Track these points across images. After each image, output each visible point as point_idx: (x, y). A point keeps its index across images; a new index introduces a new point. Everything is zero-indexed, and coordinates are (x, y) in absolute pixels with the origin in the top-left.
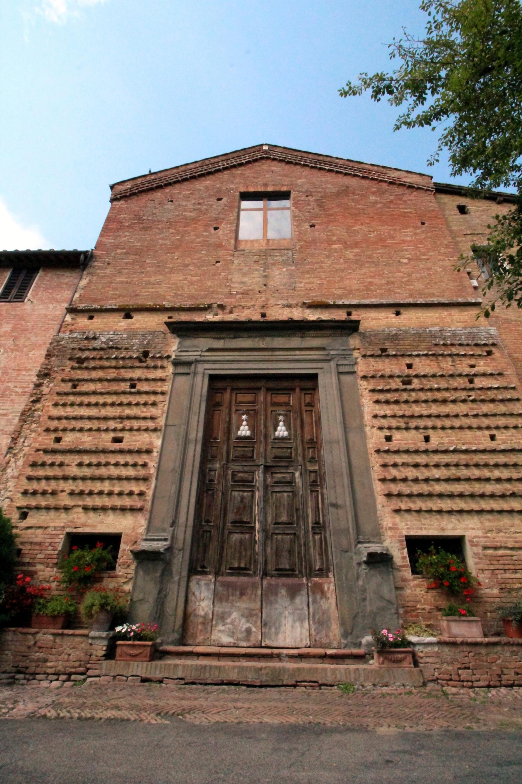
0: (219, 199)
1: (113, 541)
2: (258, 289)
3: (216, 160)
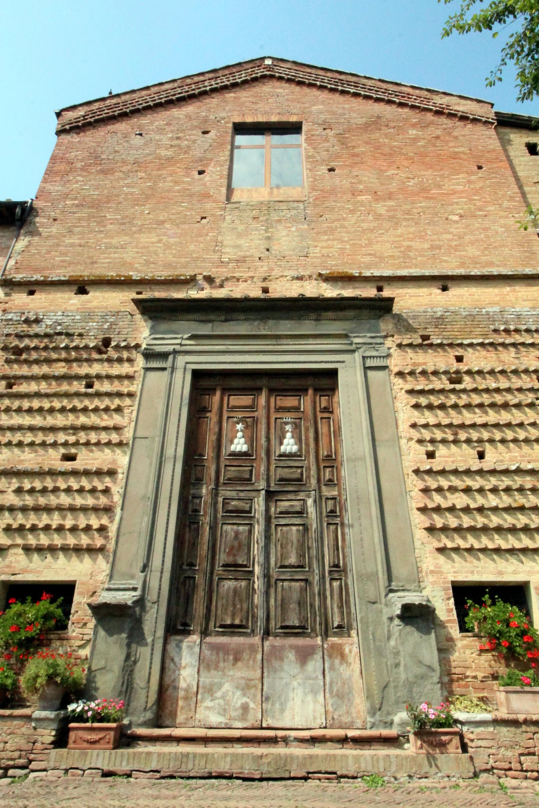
0: (205, 133)
3: (201, 78)
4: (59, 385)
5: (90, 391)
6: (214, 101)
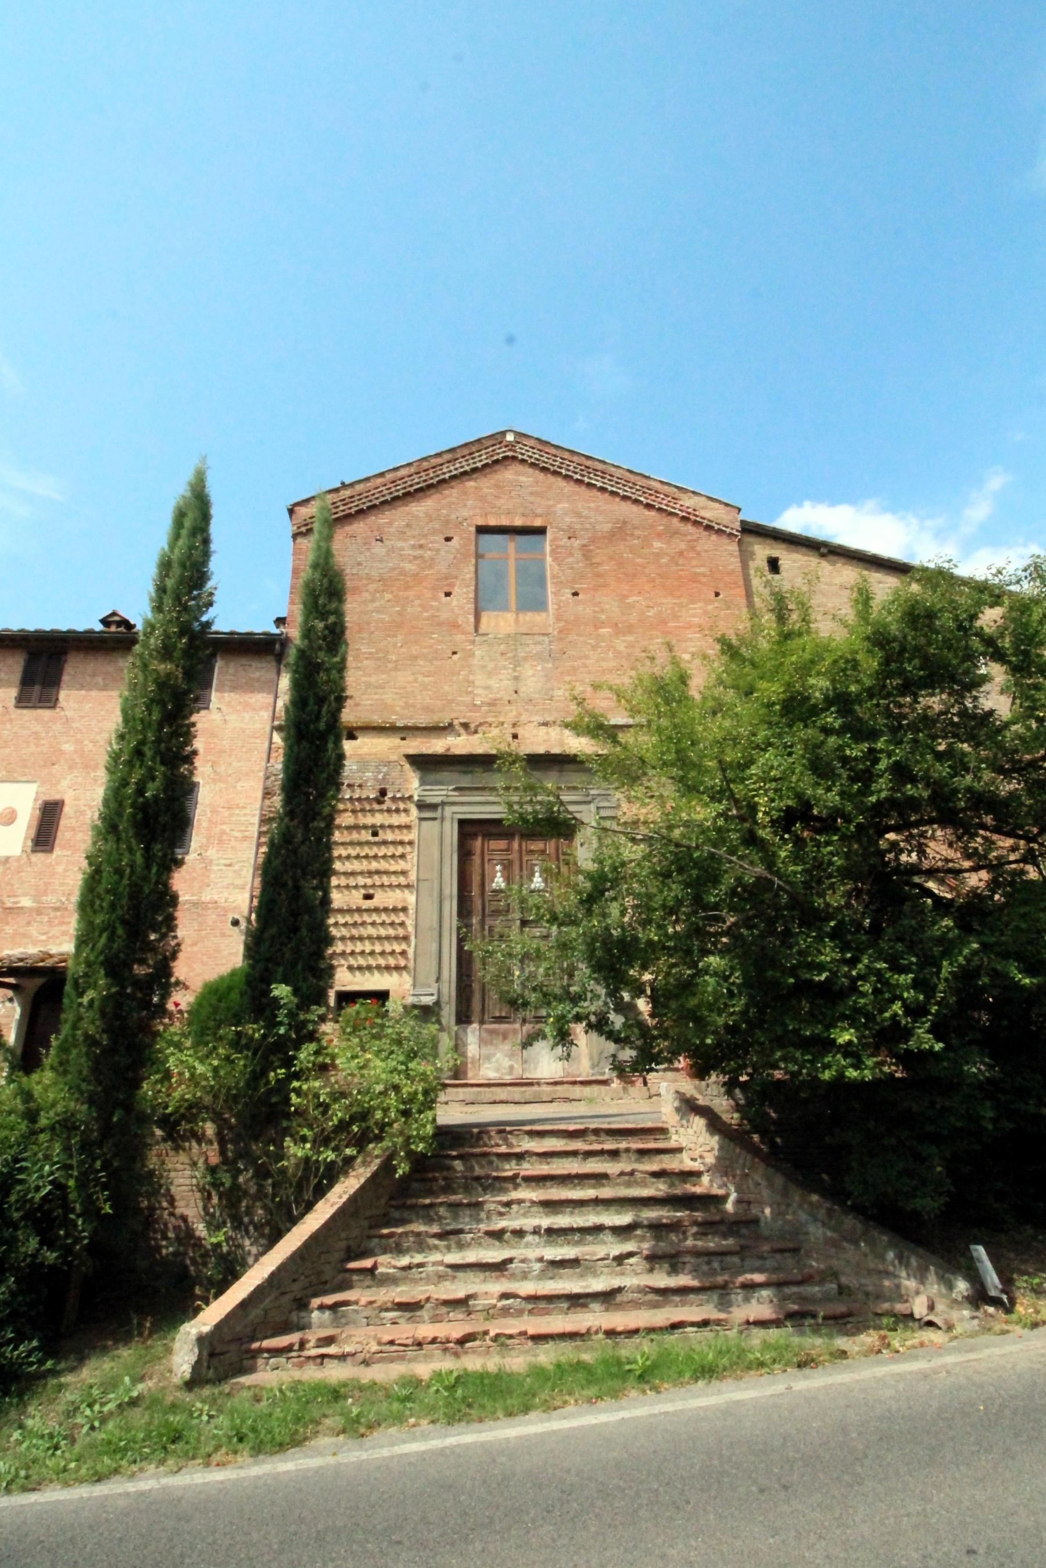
0: (448, 539)
1: (382, 996)
2: (507, 698)
3: (439, 461)
4: (350, 833)
5: (376, 839)
6: (452, 493)
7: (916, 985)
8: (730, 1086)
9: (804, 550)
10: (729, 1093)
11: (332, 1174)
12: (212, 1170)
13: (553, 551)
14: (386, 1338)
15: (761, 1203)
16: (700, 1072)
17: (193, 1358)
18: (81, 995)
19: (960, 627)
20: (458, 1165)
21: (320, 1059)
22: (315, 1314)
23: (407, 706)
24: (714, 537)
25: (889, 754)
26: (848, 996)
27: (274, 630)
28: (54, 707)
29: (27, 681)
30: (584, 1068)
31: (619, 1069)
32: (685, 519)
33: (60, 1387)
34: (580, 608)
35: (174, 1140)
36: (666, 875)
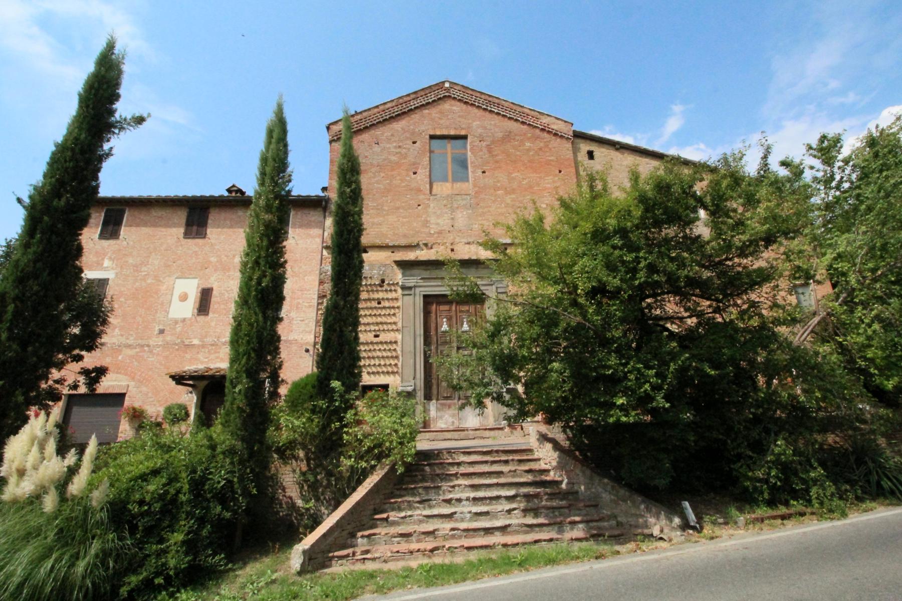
0: (414, 143)
1: (385, 387)
2: (448, 229)
3: (408, 98)
6: (416, 117)
7: (657, 375)
8: (564, 430)
9: (606, 146)
10: (564, 431)
11: (365, 474)
12: (303, 474)
13: (471, 149)
14: (395, 550)
15: (579, 484)
16: (549, 421)
17: (301, 561)
18: (234, 387)
19: (684, 192)
20: (427, 469)
21: (357, 418)
22: (360, 540)
23: (394, 234)
24: (559, 140)
25: (646, 258)
26: (623, 382)
27: (322, 195)
28: (205, 237)
29: (189, 224)
30: (491, 423)
31: (508, 419)
32: (543, 130)
33: (237, 576)
34: (486, 180)
35: (284, 460)
36: (532, 322)
